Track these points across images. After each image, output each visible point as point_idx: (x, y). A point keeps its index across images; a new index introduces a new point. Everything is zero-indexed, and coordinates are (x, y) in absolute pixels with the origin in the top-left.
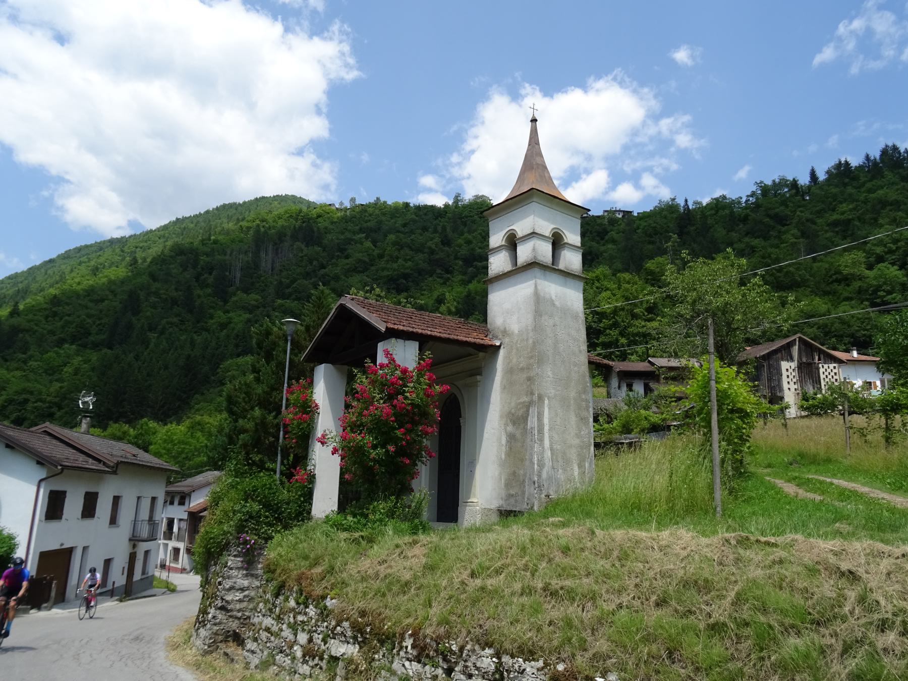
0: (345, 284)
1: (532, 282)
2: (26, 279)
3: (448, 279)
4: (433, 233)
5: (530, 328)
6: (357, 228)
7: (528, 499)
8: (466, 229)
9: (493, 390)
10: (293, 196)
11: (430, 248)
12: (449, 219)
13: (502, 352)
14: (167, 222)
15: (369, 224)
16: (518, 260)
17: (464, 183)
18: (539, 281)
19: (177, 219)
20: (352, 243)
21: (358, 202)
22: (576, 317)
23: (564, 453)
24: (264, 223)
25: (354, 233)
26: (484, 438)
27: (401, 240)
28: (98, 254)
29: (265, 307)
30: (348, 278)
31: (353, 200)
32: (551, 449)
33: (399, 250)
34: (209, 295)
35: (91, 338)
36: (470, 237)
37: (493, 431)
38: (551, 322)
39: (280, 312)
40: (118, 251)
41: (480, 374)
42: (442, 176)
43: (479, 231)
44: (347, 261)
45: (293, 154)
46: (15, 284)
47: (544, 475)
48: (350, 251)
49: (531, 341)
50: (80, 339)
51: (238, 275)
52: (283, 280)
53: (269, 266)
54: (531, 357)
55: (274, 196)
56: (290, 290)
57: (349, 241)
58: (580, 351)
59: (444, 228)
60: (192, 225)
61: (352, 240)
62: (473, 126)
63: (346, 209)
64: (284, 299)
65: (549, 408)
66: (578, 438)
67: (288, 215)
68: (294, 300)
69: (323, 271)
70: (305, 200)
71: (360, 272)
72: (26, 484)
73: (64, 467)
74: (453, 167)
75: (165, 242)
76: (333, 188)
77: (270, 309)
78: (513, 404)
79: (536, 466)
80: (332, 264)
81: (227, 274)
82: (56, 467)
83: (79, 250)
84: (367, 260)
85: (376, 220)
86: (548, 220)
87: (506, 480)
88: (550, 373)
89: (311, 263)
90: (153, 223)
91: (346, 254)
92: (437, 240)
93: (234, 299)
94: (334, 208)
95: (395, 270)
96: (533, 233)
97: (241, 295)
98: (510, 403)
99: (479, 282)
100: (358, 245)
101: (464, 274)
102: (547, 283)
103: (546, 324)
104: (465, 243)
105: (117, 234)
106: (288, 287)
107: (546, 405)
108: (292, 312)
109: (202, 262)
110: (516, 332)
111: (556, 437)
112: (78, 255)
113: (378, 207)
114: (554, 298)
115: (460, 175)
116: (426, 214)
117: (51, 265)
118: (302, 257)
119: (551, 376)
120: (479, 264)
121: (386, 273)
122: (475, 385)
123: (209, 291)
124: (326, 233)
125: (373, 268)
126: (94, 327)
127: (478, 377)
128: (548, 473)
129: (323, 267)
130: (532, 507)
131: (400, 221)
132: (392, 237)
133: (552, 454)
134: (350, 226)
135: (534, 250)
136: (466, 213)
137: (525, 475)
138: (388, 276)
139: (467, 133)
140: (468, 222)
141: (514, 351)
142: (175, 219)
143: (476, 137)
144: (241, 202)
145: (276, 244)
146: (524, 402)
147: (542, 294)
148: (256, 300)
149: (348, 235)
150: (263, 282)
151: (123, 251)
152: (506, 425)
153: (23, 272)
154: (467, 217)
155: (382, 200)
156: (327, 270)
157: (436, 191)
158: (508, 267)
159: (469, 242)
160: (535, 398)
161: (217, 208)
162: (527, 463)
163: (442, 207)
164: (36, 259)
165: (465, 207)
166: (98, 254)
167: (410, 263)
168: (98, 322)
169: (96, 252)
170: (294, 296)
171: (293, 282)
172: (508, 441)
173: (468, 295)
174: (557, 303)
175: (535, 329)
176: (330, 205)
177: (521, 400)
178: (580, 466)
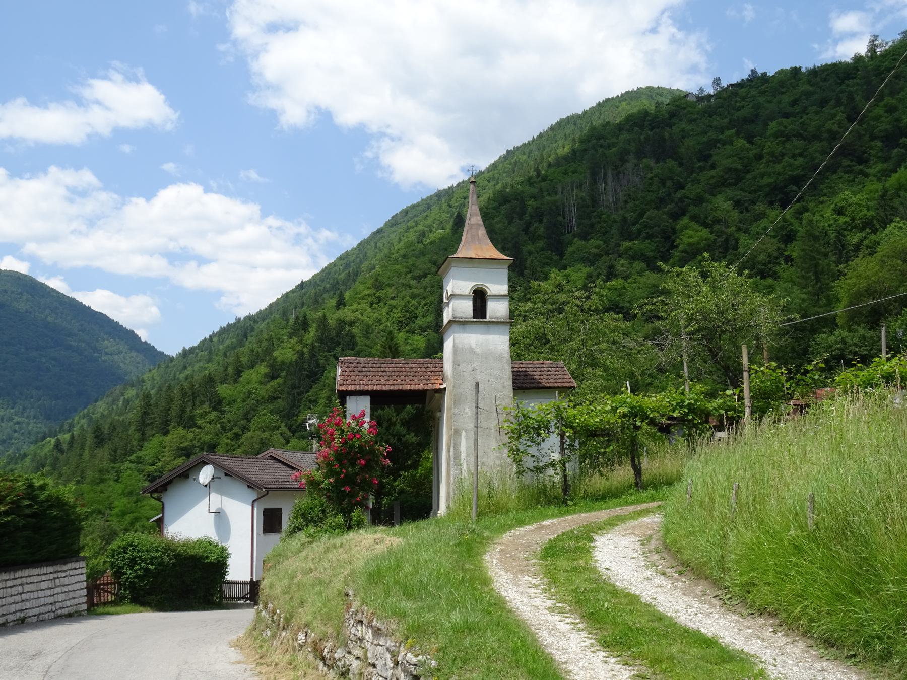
0: (710, 206)
2: (357, 258)
4: (835, 107)
6: (726, 121)
10: (648, 88)
11: (830, 131)
14: (497, 158)
18: (457, 335)
19: (508, 152)
20: (718, 145)
21: (724, 84)
22: (500, 358)
24: (602, 141)
25: (722, 130)
27: (785, 127)
28: (425, 214)
31: (717, 81)
33: (783, 143)
34: (543, 250)
35: (419, 322)
38: (470, 368)
39: (626, 259)
40: (445, 206)
44: (713, 173)
46: (347, 266)
50: (407, 325)
51: (574, 215)
55: (622, 95)
56: (638, 226)
57: (713, 144)
58: (504, 387)
60: (525, 157)
61: (718, 141)
64: (631, 240)
65: (467, 439)
69: (679, 194)
70: (665, 89)
71: (730, 185)
72: (196, 507)
73: (268, 490)
75: (495, 185)
76: (703, 66)
81: (560, 218)
82: (262, 489)
83: (406, 212)
84: (739, 167)
85: (751, 105)
89: (664, 185)
90: (483, 163)
91: (710, 163)
93: (570, 249)
95: (779, 174)
97: (578, 243)
100: (728, 147)
101: (886, 159)
102: (465, 335)
103: (464, 370)
104: (886, 112)
105: (444, 185)
106: (634, 224)
107: (463, 437)
108: (643, 255)
109: (530, 209)
112: (405, 219)
113: (757, 81)
114: (474, 346)
117: (380, 236)
118: (651, 179)
121: (767, 180)
123: (541, 244)
124: (684, 137)
125: (749, 176)
126: (420, 308)
129: (681, 187)
131: (786, 99)
132: (773, 126)
134: (717, 121)
138: (769, 185)
142: (505, 152)
144: (580, 113)
145: (616, 167)
147: (460, 346)
148: (597, 247)
149: (712, 135)
150: (605, 222)
151: (450, 206)
153: (353, 249)
155: (760, 71)
161: (552, 128)
164: (366, 232)
166: (425, 214)
167: (801, 160)
168: (423, 302)
169: (424, 211)
171: (641, 215)
173: (885, 192)
174: (478, 350)
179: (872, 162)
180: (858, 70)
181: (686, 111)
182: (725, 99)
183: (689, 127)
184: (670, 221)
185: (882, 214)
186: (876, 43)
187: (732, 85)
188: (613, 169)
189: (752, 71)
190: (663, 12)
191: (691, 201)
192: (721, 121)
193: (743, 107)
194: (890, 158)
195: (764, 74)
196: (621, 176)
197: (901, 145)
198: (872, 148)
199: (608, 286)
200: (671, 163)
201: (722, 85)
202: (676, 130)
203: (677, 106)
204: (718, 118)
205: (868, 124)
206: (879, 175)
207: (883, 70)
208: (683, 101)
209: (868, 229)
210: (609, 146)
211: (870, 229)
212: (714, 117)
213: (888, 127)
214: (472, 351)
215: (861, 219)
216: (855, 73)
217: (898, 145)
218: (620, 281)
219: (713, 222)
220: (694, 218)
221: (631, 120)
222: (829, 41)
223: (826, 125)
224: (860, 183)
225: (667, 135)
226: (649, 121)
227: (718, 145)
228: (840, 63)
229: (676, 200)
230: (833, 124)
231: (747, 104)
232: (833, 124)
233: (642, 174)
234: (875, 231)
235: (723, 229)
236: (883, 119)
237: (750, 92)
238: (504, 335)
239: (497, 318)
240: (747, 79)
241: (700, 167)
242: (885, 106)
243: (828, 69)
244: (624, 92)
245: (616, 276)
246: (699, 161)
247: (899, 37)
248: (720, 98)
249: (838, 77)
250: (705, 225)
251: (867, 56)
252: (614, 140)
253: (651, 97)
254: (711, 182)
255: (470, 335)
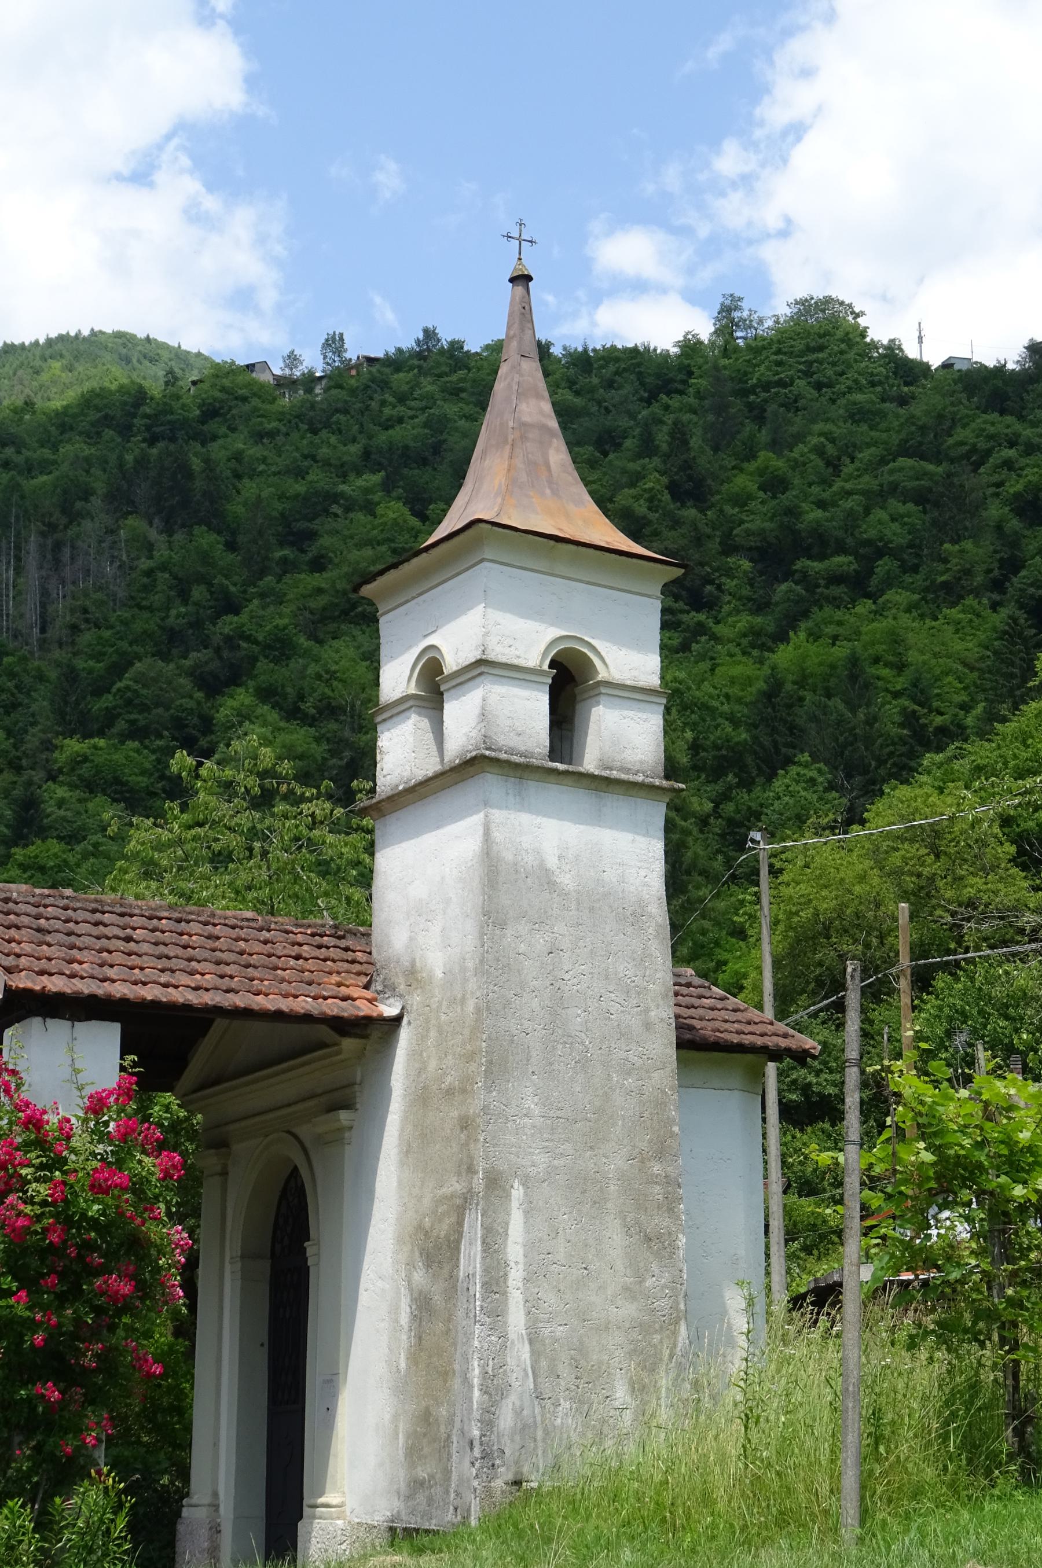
0: (312, 669)
1: (476, 820)
3: (701, 629)
4: (639, 456)
5: (470, 964)
6: (355, 449)
7: (458, 1494)
8: (764, 436)
9: (382, 1156)
10: (119, 335)
12: (699, 395)
13: (405, 1035)
15: (397, 433)
16: (445, 753)
17: (768, 252)
18: (498, 815)
20: (335, 509)
21: (352, 353)
22: (637, 916)
23: (581, 1350)
25: (343, 471)
26: (359, 1308)
29: (18, 769)
30: (320, 642)
31: (334, 344)
32: (533, 1338)
36: (778, 464)
37: (380, 1284)
38: (540, 942)
39: (73, 787)
41: (348, 1105)
42: (685, 232)
43: (814, 440)
44: (318, 580)
45: (119, 177)
47: (506, 1420)
48: (326, 541)
49: (470, 1006)
52: (80, 663)
53: (32, 615)
54: (470, 1057)
55: (50, 342)
56: (107, 701)
58: (648, 1026)
59: (680, 436)
61: (335, 497)
62: (789, 32)
63: (310, 380)
65: (527, 1213)
66: (634, 1298)
67: (93, 416)
68: (124, 737)
69: (228, 624)
70: (165, 346)
74: (723, 194)
76: (268, 298)
77: (38, 776)
78: (427, 1201)
79: (476, 1393)
80: (262, 595)
85: (422, 418)
86: (537, 614)
87: (408, 1437)
88: (530, 1103)
89: (184, 595)
91: (313, 551)
92: (654, 481)
94: (265, 378)
96: (480, 662)
98: (420, 1198)
99: (814, 636)
100: (360, 517)
101: (761, 607)
102: (525, 819)
103: (522, 948)
104: (762, 488)
106: (99, 692)
107: (515, 1204)
108: (117, 781)
110: (439, 974)
111: (550, 1299)
114: (552, 862)
115: (750, 224)
116: (610, 385)
118: (149, 573)
119: (537, 1111)
120: (817, 566)
122: (336, 1138)
124: (238, 476)
127: (344, 1116)
128: (518, 1413)
130: (466, 1518)
133: (536, 1355)
135: (484, 715)
136: (762, 372)
137: (450, 1421)
139: (771, 63)
140: (772, 408)
141: (433, 1033)
143: (807, 73)
146: (452, 1196)
147: (508, 856)
149: (318, 478)
152: (410, 1265)
154: (766, 386)
155: (446, 336)
156: (244, 617)
157: (662, 290)
158: (430, 766)
159: (775, 485)
160: (479, 1182)
162: (457, 1383)
163: (674, 350)
165: (758, 348)
170: (121, 725)
171: (118, 669)
172: (414, 1317)
174: (566, 880)
175: (482, 968)
176: (251, 367)
177: (446, 1191)
178: (638, 1388)
179: (726, 608)
180: (690, 374)
181: (246, 408)
182: (353, 392)
183: (255, 451)
184: (199, 695)
185: (766, 741)
186: (736, 314)
187: (370, 360)
188: (43, 534)
189: (426, 331)
190: (169, 137)
191: (256, 649)
192: (341, 448)
193: (400, 420)
194: (768, 604)
195: (456, 346)
196: (66, 553)
197: (797, 576)
198: (729, 573)
199: (20, 858)
200: (206, 539)
201: (347, 355)
202: (218, 451)
203: (223, 389)
204: (333, 439)
205: (721, 511)
206: (745, 642)
207: (754, 386)
208: (240, 379)
209: (730, 777)
210: (29, 469)
211: (736, 775)
212: (324, 434)
213: (768, 525)
214: (546, 880)
215: (717, 748)
216: (684, 382)
217: (788, 575)
218: (54, 846)
219: (320, 712)
220: (267, 694)
221: (98, 409)
222: (581, 294)
223: (618, 498)
224: (702, 657)
225: (196, 464)
226: (146, 416)
227: (335, 509)
228: (647, 349)
229: (216, 640)
230: (637, 498)
231: (410, 413)
232: (637, 498)
233: (124, 558)
234: (747, 784)
235: (347, 733)
236: (752, 505)
237: (418, 385)
238: (647, 834)
239: (628, 771)
240: (411, 351)
241: (284, 560)
242: (761, 472)
243: (617, 360)
244: (53, 335)
245: (43, 833)
246: (282, 544)
247: (788, 311)
248: (340, 386)
249: (642, 384)
250: (293, 713)
251: (712, 343)
252: (46, 453)
253: (128, 360)
254: (313, 604)
255: (540, 820)
